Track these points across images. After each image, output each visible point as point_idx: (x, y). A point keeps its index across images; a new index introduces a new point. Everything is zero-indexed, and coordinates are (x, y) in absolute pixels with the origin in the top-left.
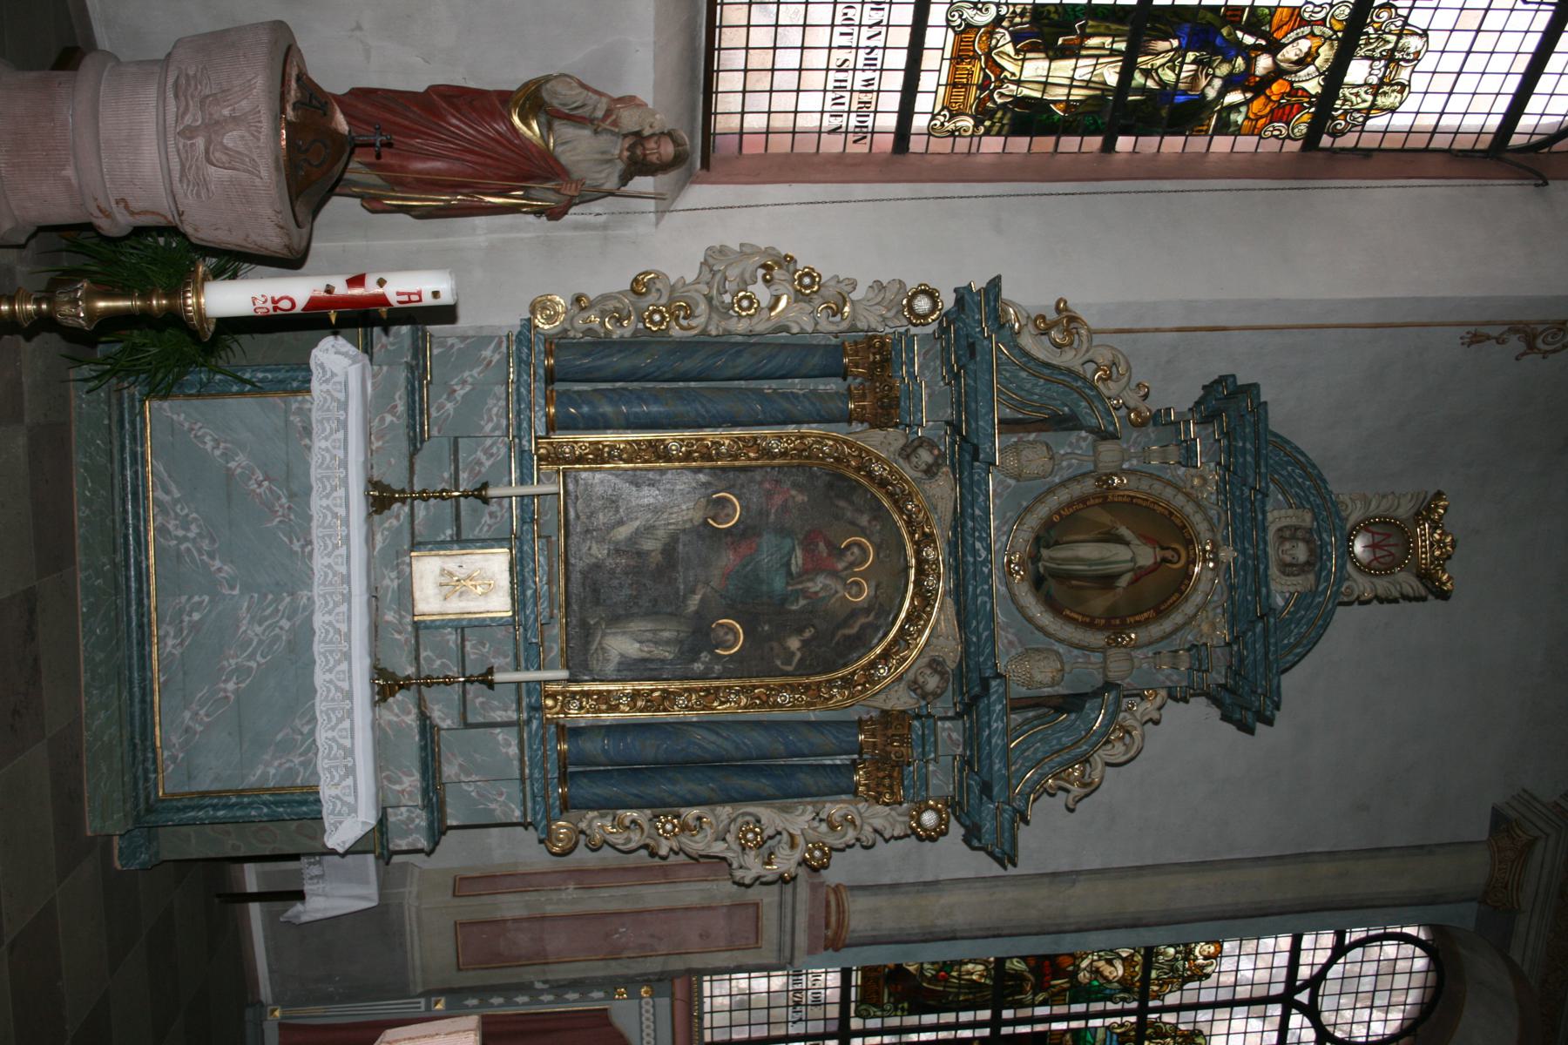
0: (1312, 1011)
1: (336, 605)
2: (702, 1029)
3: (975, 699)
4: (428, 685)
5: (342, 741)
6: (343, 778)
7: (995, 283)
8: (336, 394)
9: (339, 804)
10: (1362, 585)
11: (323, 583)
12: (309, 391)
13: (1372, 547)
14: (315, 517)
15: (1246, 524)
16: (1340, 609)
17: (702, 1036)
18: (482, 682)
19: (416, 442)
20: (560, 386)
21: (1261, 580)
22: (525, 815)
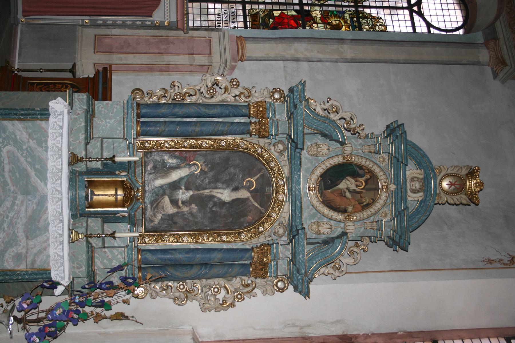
0: (421, 15)
1: (59, 267)
2: (188, 20)
3: (294, 237)
4: (91, 238)
5: (59, 253)
6: (57, 202)
7: (306, 295)
8: (59, 231)
9: (55, 147)
10: (444, 198)
11: (52, 194)
12: (48, 231)
13: (451, 184)
14: (50, 213)
15: (399, 178)
16: (435, 206)
17: (188, 23)
18: (111, 237)
19: (88, 140)
20: (142, 120)
21: (404, 199)
22: (124, 136)
